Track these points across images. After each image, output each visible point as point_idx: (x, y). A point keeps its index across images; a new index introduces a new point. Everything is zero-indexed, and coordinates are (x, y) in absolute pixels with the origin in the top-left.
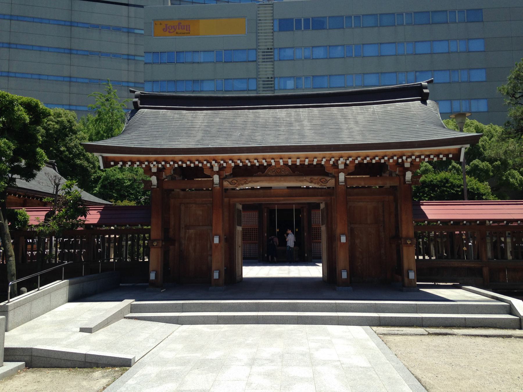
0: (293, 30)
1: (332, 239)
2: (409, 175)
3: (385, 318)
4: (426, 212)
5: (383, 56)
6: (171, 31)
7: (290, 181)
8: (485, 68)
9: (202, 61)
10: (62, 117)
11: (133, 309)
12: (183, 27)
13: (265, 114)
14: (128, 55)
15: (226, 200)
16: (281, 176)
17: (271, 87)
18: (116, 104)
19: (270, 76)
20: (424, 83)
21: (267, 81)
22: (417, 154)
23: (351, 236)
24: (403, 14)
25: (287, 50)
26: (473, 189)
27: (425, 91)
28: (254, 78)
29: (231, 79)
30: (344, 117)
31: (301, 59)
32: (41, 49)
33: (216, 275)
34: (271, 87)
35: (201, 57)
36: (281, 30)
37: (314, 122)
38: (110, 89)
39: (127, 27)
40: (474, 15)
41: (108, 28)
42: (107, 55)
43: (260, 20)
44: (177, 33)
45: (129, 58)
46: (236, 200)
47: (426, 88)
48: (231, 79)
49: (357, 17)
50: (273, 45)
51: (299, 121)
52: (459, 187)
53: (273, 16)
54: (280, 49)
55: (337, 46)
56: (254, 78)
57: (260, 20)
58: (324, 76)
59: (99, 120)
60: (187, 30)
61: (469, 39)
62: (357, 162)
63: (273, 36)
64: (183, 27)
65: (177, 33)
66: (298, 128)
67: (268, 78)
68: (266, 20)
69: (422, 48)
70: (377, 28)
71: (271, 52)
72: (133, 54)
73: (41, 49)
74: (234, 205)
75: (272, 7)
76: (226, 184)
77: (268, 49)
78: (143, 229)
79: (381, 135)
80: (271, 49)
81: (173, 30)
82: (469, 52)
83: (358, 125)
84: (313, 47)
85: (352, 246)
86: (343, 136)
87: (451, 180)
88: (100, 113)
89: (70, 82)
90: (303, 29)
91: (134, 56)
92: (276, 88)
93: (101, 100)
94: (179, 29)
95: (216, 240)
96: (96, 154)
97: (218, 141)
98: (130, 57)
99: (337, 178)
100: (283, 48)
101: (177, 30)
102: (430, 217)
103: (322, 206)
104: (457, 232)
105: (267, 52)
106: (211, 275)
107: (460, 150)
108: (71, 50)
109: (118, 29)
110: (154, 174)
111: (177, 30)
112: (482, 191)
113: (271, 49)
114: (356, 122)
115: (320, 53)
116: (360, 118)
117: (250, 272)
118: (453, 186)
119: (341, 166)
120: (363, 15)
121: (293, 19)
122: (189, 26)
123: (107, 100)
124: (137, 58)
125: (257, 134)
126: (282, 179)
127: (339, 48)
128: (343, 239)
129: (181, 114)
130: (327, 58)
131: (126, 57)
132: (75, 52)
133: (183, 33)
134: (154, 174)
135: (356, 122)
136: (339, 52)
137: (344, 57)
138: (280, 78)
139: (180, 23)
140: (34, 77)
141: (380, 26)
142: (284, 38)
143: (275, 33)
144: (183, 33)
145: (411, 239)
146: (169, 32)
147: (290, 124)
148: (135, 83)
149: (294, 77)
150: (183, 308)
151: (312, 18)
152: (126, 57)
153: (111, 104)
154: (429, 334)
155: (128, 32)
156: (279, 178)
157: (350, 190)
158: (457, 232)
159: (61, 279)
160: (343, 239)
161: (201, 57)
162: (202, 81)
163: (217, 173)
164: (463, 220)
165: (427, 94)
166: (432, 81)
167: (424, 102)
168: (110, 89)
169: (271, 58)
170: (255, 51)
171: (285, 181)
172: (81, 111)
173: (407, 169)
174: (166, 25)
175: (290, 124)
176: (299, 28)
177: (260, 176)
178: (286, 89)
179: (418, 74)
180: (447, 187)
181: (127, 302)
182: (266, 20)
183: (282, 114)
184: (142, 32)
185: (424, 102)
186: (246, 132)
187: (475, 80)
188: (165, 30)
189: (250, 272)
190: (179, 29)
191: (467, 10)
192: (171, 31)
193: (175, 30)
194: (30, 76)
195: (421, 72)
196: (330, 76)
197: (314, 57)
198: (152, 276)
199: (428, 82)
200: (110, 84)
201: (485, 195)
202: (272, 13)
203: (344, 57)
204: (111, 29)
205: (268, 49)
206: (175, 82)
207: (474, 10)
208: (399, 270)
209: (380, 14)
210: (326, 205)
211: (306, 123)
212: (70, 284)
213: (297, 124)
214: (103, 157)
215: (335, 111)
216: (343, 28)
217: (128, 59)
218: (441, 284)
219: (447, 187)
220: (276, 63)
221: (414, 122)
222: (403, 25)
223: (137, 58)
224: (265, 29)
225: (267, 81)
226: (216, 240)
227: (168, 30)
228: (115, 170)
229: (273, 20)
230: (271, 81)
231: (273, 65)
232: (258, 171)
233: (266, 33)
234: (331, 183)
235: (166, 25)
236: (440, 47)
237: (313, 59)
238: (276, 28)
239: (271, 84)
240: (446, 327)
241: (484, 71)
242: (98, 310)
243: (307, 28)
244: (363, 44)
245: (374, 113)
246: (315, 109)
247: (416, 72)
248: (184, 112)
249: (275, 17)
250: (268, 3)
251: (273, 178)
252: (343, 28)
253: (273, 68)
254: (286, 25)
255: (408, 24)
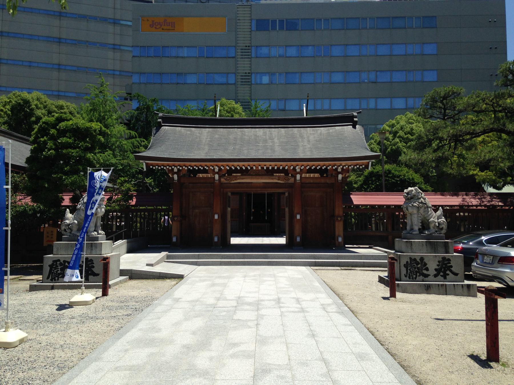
0: (268, 30)
1: (292, 217)
2: (340, 177)
3: (318, 262)
4: (353, 199)
5: (348, 56)
6: (158, 27)
7: (265, 179)
8: (437, 70)
9: (186, 55)
10: (64, 109)
11: (168, 257)
12: (168, 24)
13: (249, 132)
14: (114, 45)
15: (222, 190)
16: (259, 175)
17: (249, 82)
18: (110, 97)
19: (247, 72)
20: (355, 114)
21: (245, 76)
22: (343, 164)
23: (304, 214)
24: (367, 19)
25: (263, 48)
26: (409, 179)
27: (355, 119)
28: (233, 73)
29: (213, 73)
30: (302, 136)
31: (275, 57)
32: (31, 37)
33: (216, 239)
34: (249, 82)
35: (185, 52)
36: (257, 30)
37: (281, 140)
38: (103, 82)
39: (113, 18)
40: (429, 22)
41: (95, 18)
42: (94, 44)
43: (239, 20)
44: (163, 29)
45: (115, 47)
46: (228, 190)
47: (356, 117)
48: (213, 73)
49: (326, 20)
50: (250, 43)
51: (271, 139)
52: (398, 177)
53: (250, 17)
54: (257, 46)
55: (308, 46)
56: (233, 73)
57: (239, 20)
58: (296, 73)
59: (94, 110)
60: (172, 27)
61: (423, 43)
62: (307, 168)
63: (250, 34)
64: (168, 24)
65: (163, 29)
66: (271, 144)
67: (246, 73)
68: (244, 20)
69: (383, 50)
70: (344, 31)
71: (249, 49)
72: (119, 44)
73: (31, 37)
74: (227, 193)
75: (251, 8)
76: (222, 180)
77: (246, 46)
78: (157, 209)
79: (323, 151)
80: (249, 47)
81: (159, 26)
82: (423, 55)
83: (310, 144)
84: (286, 46)
85: (304, 222)
86: (299, 151)
87: (393, 171)
88: (93, 104)
89: (59, 69)
90: (278, 29)
91: (120, 45)
92: (253, 82)
93: (96, 92)
94: (164, 25)
95: (216, 217)
96: (141, 161)
97: (219, 153)
98: (116, 47)
99: (295, 177)
100: (260, 46)
101: (163, 27)
102: (355, 203)
103: (287, 194)
104: (397, 213)
105: (245, 49)
106: (213, 239)
107: (369, 163)
108: (60, 39)
109: (104, 20)
110: (176, 173)
111: (163, 27)
112: (416, 181)
113: (249, 47)
114: (309, 141)
115: (292, 52)
116: (311, 138)
117: (235, 241)
118: (394, 176)
119: (298, 170)
120: (331, 19)
121: (268, 20)
122: (174, 23)
123: (101, 92)
124: (122, 48)
125: (244, 148)
126: (260, 177)
127: (310, 48)
128: (298, 217)
129: (191, 131)
130: (298, 57)
131: (112, 46)
132: (64, 41)
133: (168, 30)
134: (176, 173)
135: (309, 141)
136: (309, 51)
137: (314, 57)
138: (257, 73)
139: (165, 20)
140: (25, 64)
141: (347, 29)
142: (260, 37)
143: (253, 33)
144: (168, 30)
145: (340, 217)
146: (156, 28)
147: (265, 141)
148: (120, 71)
149: (269, 73)
150: (199, 257)
151: (286, 20)
152: (112, 46)
153: (104, 96)
154: (342, 269)
155: (114, 23)
156: (258, 177)
157: (303, 184)
158: (397, 213)
159: (122, 239)
160: (298, 217)
161: (185, 52)
162: (186, 74)
163: (217, 173)
164: (376, 205)
165: (356, 121)
166: (360, 112)
167: (354, 127)
168: (103, 82)
169: (249, 55)
170: (234, 48)
171: (262, 179)
172: (70, 97)
173: (340, 173)
174: (153, 21)
175: (265, 141)
176: (274, 28)
177: (245, 175)
178: (261, 84)
179: (378, 73)
180: (389, 177)
181: (164, 254)
182: (244, 20)
183: (260, 132)
184: (130, 23)
185: (354, 127)
186: (237, 147)
187: (427, 80)
188: (151, 26)
189: (235, 241)
190: (164, 25)
191: (423, 17)
192: (158, 27)
193: (161, 26)
194: (21, 63)
195: (381, 71)
196: (301, 73)
197: (287, 56)
198: (174, 239)
199: (357, 113)
200: (103, 78)
201: (418, 183)
202: (250, 14)
203: (314, 57)
204: (98, 19)
205: (246, 46)
206: (161, 74)
207: (429, 17)
208: (334, 237)
209: (347, 18)
210: (289, 193)
211: (276, 140)
212: (128, 242)
213: (270, 141)
214: (146, 163)
215: (295, 131)
216: (314, 30)
217: (114, 49)
218: (361, 246)
219: (389, 177)
220: (253, 59)
221: (346, 142)
222: (366, 28)
223: (122, 48)
224: (243, 29)
225: (245, 76)
226: (216, 217)
227: (155, 26)
228: (109, 156)
229: (251, 20)
230: (249, 76)
231: (250, 61)
232: (245, 172)
233: (244, 32)
234: (292, 180)
235: (153, 21)
236: (398, 50)
237: (287, 57)
238: (254, 28)
239: (249, 79)
240: (352, 266)
241: (435, 72)
242: (149, 257)
243: (281, 28)
244: (331, 45)
245: (321, 134)
246: (282, 129)
247: (377, 71)
248: (193, 129)
249: (253, 17)
250: (246, 4)
251: (254, 177)
252: (314, 30)
253: (250, 64)
254: (263, 25)
255: (370, 28)
